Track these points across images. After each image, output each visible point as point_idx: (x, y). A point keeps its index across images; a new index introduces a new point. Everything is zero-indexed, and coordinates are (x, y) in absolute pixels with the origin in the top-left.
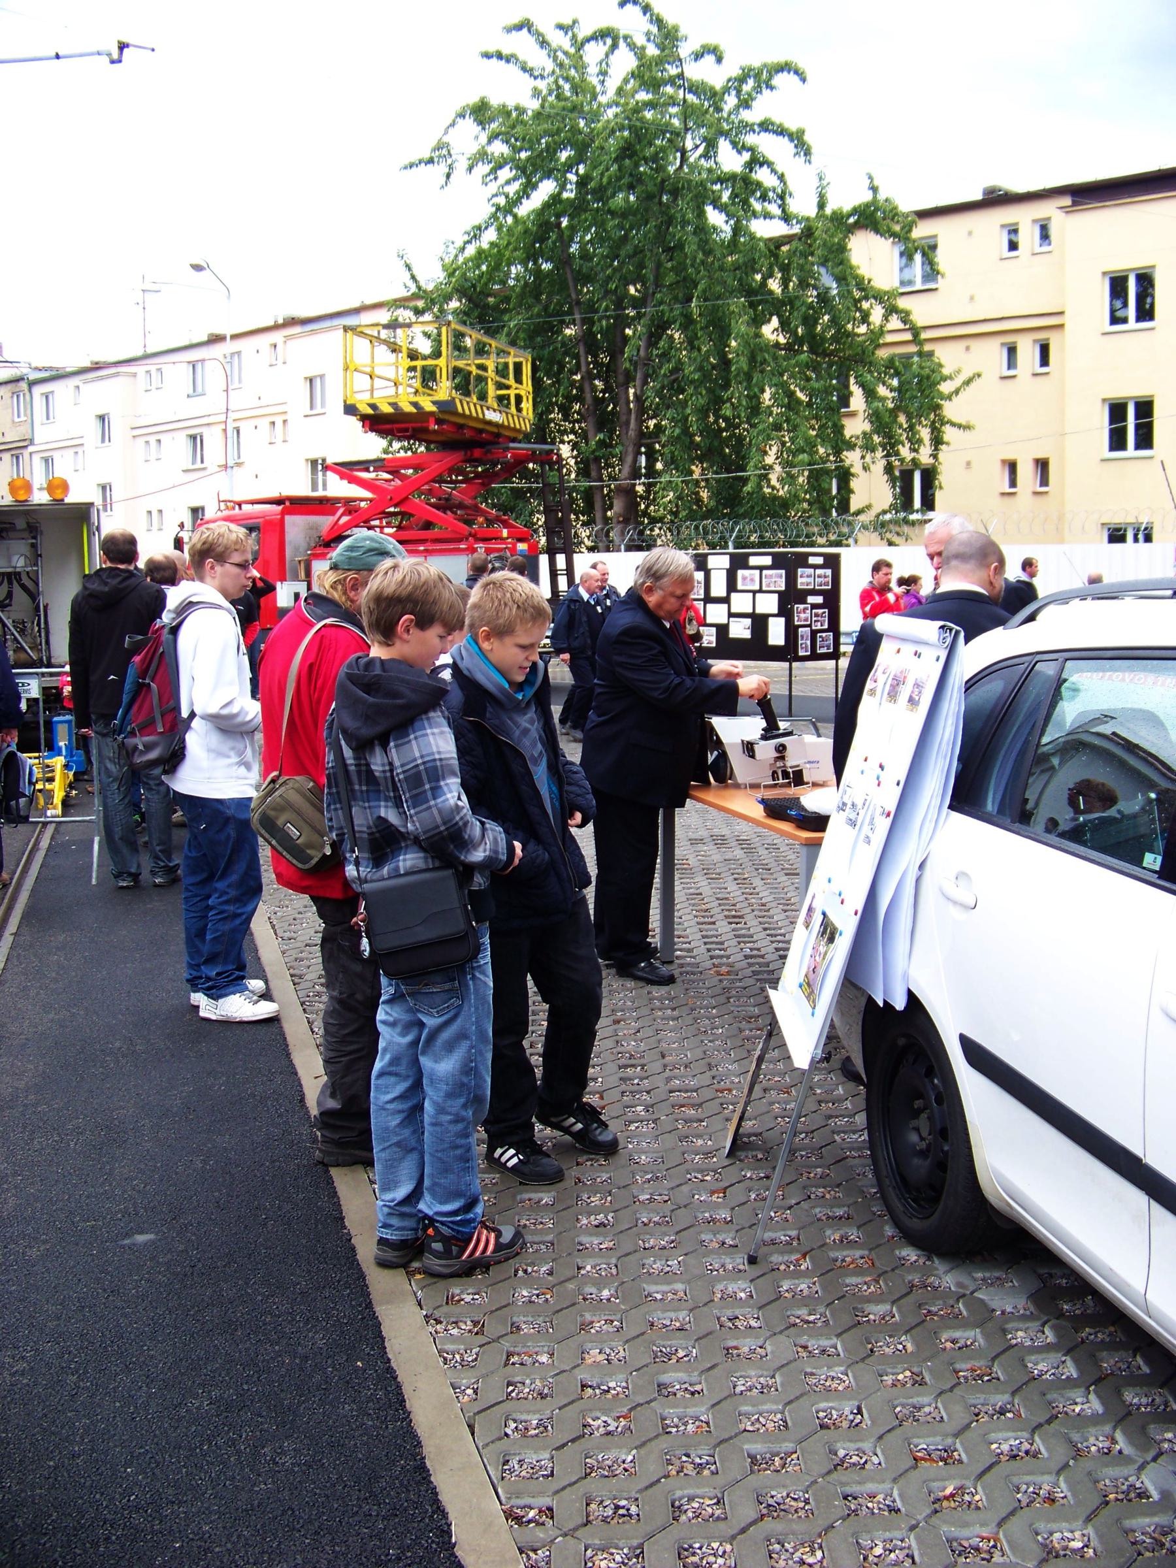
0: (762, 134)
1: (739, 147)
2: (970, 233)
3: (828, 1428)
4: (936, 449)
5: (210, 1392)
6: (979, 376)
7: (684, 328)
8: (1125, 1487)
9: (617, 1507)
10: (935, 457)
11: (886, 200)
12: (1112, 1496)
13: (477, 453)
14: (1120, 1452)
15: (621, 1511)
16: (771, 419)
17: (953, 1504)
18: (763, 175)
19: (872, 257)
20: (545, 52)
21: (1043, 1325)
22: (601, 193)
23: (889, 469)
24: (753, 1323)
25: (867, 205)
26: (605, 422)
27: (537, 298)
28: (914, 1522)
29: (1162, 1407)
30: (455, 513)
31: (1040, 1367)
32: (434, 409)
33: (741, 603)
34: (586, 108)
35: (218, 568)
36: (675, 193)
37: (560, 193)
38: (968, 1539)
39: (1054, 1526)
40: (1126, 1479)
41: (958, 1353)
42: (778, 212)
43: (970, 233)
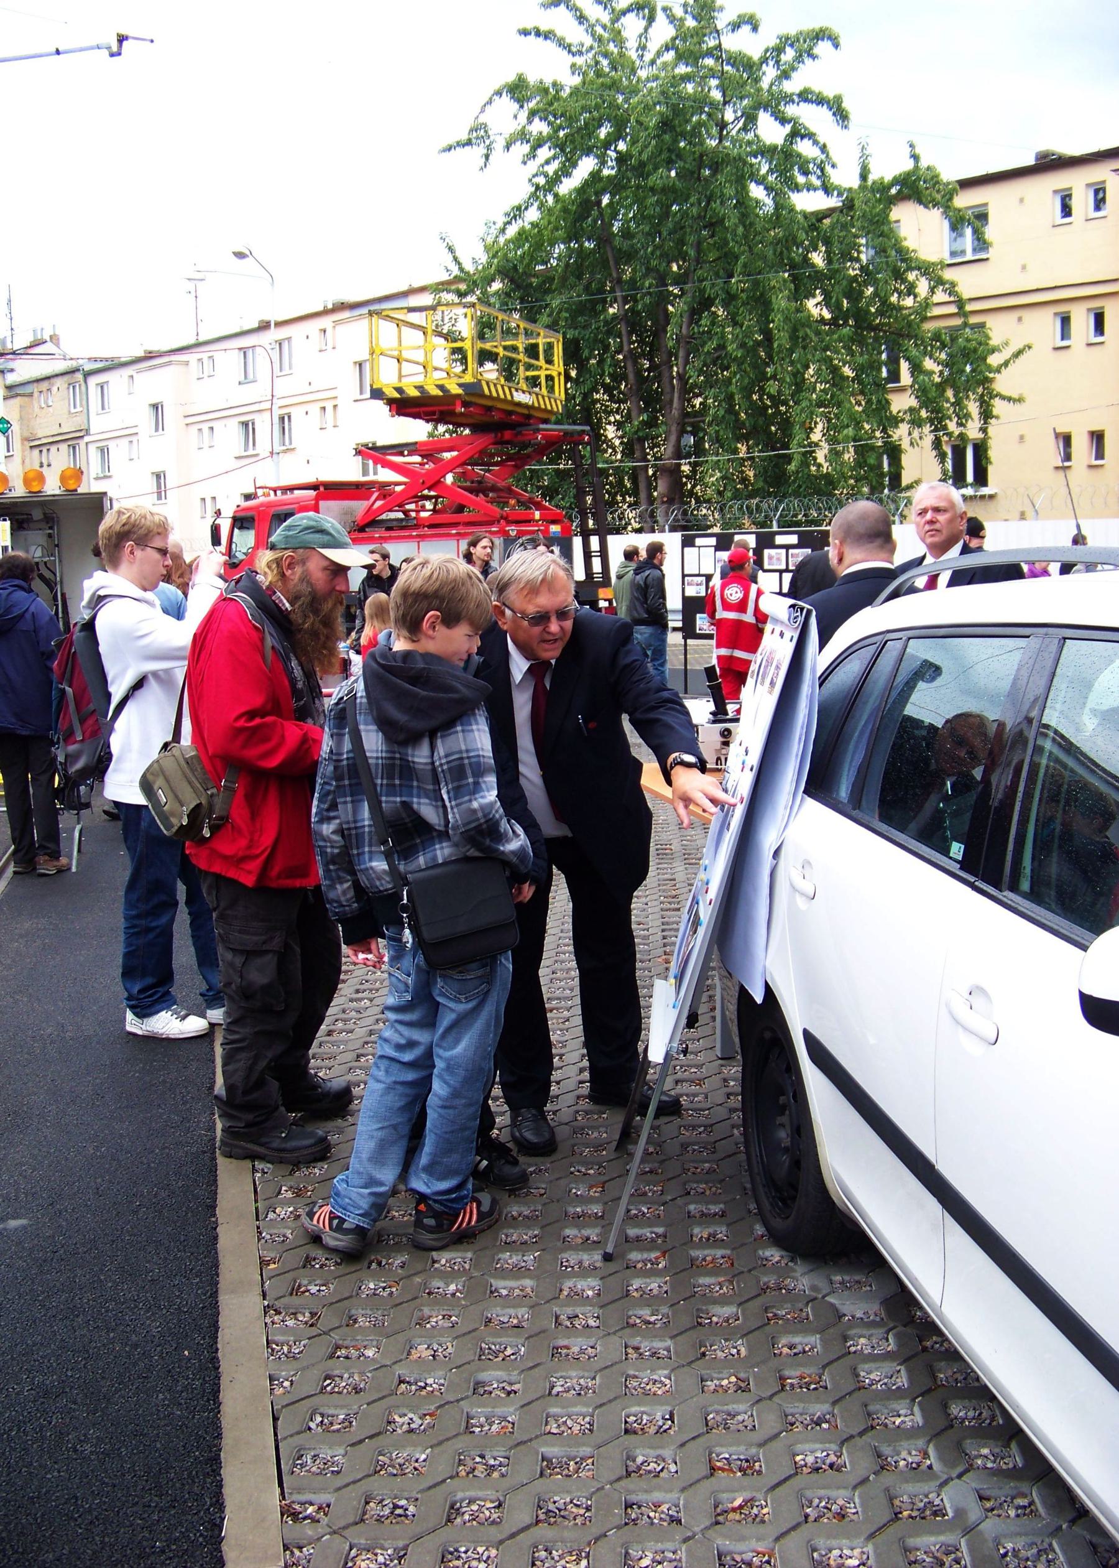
0: (801, 104)
1: (783, 120)
2: (1021, 200)
3: (635, 1433)
4: (985, 423)
5: (34, 1377)
6: (1030, 347)
7: (726, 306)
8: (922, 1505)
9: (396, 1507)
10: (984, 430)
11: (928, 168)
12: (906, 1514)
13: (508, 435)
14: (930, 1467)
15: (399, 1511)
16: (814, 396)
17: (738, 1517)
18: (804, 148)
19: (920, 230)
20: (583, 28)
21: (887, 1333)
22: (641, 170)
23: (937, 444)
24: (591, 1322)
25: (908, 175)
26: (652, 401)
27: (579, 277)
28: (689, 1534)
29: (988, 1421)
30: (487, 496)
31: (872, 1376)
32: (460, 391)
34: (625, 82)
35: (138, 553)
36: (716, 168)
37: (600, 171)
38: (741, 1553)
39: (834, 1543)
40: (926, 1496)
41: (790, 1360)
42: (818, 183)
43: (1021, 200)
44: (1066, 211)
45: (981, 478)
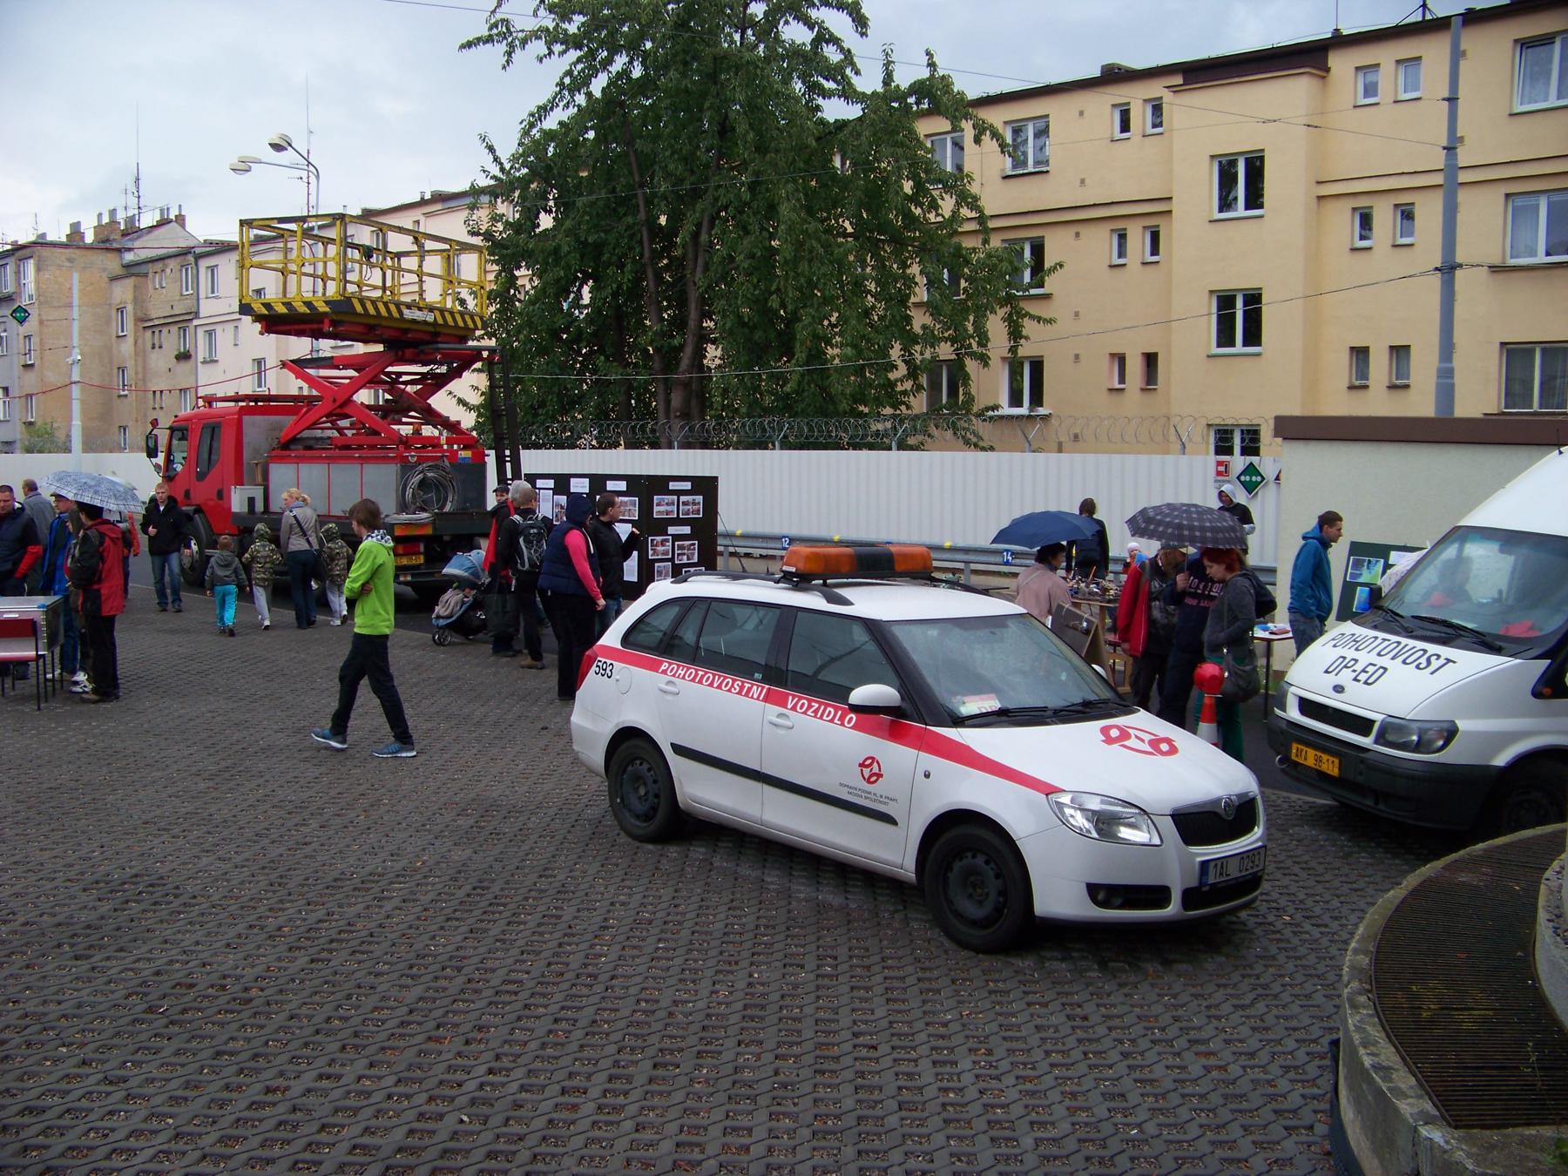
2: (1081, 113)
18: (832, 54)
43: (1081, 113)
44: (1125, 127)
45: (1037, 399)
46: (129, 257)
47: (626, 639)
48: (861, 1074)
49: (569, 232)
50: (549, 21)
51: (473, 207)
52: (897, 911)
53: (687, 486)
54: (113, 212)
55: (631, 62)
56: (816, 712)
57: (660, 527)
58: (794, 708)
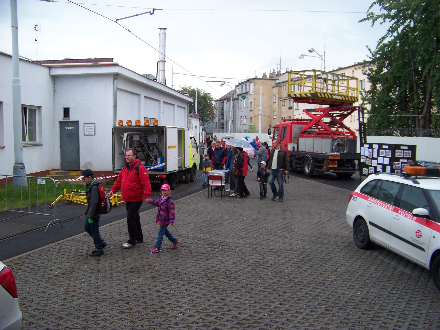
33: (380, 160)
46: (277, 81)
47: (361, 190)
48: (385, 323)
49: (391, 73)
50: (386, 12)
51: (364, 67)
52: (426, 278)
53: (406, 148)
54: (274, 70)
55: (410, 22)
56: (406, 215)
57: (398, 159)
58: (400, 214)
